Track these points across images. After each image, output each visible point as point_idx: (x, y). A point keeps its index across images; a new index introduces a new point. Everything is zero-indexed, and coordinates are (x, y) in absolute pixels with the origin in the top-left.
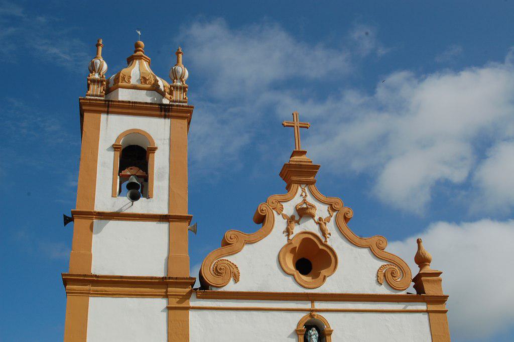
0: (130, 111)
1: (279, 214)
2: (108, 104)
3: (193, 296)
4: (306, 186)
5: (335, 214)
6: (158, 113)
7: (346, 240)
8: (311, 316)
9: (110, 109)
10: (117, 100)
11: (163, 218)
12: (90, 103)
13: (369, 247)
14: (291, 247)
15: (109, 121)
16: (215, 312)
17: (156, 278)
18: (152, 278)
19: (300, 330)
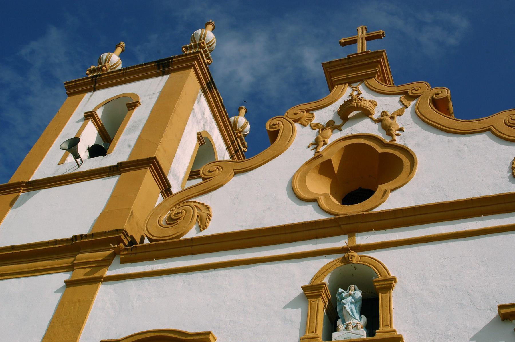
0: (121, 80)
1: (305, 126)
2: (96, 79)
3: (116, 260)
4: (361, 84)
5: (413, 103)
6: (155, 72)
7: (434, 130)
8: (346, 261)
9: (98, 85)
10: (216, 160)
11: (114, 171)
12: (75, 84)
13: (489, 130)
14: (320, 161)
15: (92, 97)
16: (146, 281)
17: (62, 241)
18: (56, 242)
19: (351, 312)
